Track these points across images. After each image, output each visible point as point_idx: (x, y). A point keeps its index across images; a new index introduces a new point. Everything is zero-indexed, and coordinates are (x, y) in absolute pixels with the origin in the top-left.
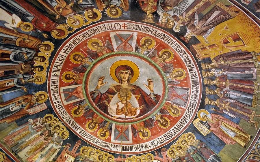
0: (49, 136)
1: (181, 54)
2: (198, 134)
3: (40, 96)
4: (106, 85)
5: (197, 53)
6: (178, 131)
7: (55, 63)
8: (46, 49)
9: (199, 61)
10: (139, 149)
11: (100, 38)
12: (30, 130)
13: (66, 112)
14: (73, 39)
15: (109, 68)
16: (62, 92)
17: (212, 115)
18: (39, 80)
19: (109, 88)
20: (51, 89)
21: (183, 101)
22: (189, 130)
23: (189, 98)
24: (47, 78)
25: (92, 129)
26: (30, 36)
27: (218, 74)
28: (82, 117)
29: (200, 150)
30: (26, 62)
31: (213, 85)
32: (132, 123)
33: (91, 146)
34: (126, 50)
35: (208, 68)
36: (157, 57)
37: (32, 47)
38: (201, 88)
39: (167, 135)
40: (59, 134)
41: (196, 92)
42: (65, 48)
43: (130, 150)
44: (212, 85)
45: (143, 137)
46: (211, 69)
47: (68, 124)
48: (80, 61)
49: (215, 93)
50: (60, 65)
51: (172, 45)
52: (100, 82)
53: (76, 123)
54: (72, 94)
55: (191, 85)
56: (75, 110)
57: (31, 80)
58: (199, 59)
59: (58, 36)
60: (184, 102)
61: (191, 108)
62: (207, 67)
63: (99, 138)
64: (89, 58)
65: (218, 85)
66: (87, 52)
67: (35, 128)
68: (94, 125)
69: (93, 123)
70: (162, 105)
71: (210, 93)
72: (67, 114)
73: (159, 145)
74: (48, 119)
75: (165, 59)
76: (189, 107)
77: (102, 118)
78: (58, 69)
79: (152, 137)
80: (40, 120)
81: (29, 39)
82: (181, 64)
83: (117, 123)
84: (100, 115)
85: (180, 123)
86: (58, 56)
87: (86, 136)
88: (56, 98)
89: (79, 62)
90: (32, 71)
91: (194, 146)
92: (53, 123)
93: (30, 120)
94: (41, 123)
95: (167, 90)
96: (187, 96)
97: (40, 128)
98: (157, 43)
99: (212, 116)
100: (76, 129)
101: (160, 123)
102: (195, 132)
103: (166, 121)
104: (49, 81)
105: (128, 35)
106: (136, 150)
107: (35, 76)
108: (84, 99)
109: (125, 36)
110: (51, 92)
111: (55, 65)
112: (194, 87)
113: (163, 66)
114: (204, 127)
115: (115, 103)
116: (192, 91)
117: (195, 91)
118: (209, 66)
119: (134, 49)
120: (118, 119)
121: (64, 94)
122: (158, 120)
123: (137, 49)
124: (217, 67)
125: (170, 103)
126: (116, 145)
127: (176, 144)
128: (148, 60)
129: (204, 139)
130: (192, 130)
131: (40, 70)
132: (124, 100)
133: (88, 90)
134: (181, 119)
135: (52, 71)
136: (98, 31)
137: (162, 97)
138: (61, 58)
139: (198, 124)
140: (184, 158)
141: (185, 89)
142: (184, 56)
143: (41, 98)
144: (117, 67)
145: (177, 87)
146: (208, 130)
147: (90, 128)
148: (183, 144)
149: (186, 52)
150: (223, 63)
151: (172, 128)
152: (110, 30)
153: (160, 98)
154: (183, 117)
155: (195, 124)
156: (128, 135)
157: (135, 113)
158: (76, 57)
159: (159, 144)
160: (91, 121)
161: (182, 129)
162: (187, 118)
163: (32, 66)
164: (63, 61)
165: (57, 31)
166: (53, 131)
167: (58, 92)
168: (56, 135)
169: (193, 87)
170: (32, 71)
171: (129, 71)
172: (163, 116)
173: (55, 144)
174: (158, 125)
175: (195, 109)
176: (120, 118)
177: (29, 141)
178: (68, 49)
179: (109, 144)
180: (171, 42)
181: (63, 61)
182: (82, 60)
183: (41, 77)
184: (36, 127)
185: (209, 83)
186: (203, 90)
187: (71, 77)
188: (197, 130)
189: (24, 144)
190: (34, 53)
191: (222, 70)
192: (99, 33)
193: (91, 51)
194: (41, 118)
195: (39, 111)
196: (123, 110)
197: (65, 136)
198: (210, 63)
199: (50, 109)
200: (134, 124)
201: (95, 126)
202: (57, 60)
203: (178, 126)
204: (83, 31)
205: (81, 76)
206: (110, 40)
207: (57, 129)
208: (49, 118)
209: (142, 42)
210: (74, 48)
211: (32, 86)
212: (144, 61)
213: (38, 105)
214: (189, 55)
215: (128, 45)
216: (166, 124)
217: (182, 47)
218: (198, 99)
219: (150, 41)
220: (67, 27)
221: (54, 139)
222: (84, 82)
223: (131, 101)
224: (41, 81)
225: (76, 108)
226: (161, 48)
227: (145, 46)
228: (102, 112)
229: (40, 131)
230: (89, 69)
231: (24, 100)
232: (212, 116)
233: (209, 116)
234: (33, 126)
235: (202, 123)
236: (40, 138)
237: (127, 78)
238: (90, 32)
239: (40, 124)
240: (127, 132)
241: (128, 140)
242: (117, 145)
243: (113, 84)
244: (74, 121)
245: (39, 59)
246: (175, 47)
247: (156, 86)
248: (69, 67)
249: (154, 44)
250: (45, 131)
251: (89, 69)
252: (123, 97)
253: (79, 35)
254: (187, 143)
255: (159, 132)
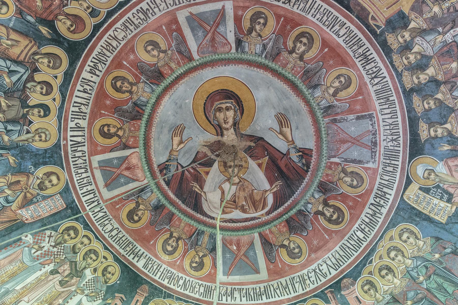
0: (71, 276)
1: (334, 29)
2: (425, 223)
3: (48, 177)
4: (190, 144)
5: (369, 13)
6: (371, 230)
7: (75, 99)
8: (51, 65)
9: (378, 31)
10: (287, 290)
11: (158, 30)
12: (26, 260)
13: (111, 217)
14: (105, 38)
15: (189, 101)
16: (96, 168)
17: (446, 163)
18: (43, 138)
19: (198, 152)
20: (71, 160)
21: (366, 150)
22: (399, 219)
23: (380, 138)
24: (60, 132)
25: (171, 253)
26: (11, 31)
27: (432, 47)
28: (146, 227)
29: (441, 263)
30: (8, 94)
31: (429, 82)
32: (261, 230)
33: (170, 296)
34: (218, 51)
35: (405, 41)
36: (285, 54)
37: (19, 59)
38: (400, 102)
39: (349, 245)
40: (95, 270)
41: (391, 118)
42: (92, 61)
43: (264, 297)
44: (425, 85)
45: (291, 258)
46: (413, 39)
47: (118, 247)
48: (127, 92)
49: (440, 103)
50: (85, 103)
51: (311, 14)
52: (176, 140)
53: (135, 243)
54: (119, 172)
55: (377, 103)
56: (129, 212)
57: (24, 137)
58: (378, 27)
59: (71, 32)
60: (370, 151)
61: (388, 161)
62: (401, 40)
63: (187, 275)
64: (145, 82)
65: (440, 78)
66: (137, 68)
67: (38, 256)
68: (174, 244)
69: (172, 240)
70: (320, 174)
71: (426, 106)
72: (111, 222)
73: (334, 273)
74: (69, 235)
75: (304, 53)
76: (384, 161)
77: (192, 224)
78: (82, 112)
79: (313, 256)
80: (50, 237)
81: (10, 37)
82: (341, 54)
83: (226, 233)
84: (185, 218)
85: (373, 208)
86: (79, 83)
87: (159, 274)
88: (85, 182)
89: (126, 96)
90: (25, 116)
91: (422, 257)
92: (82, 243)
93: (26, 236)
94: (53, 244)
95: (323, 132)
96: (373, 134)
97: (51, 256)
98: (278, 17)
99: (449, 166)
100: (136, 259)
101: (325, 218)
102: (415, 221)
103: (337, 209)
104: (64, 139)
105: (214, 11)
106: (280, 295)
107: (33, 128)
108: (146, 181)
109: (208, 15)
110: (72, 166)
111: (75, 102)
112: (384, 107)
113: (304, 74)
114: (436, 201)
115: (215, 186)
116: (381, 117)
117: (389, 116)
118: (404, 34)
119: (234, 46)
120: (226, 224)
121: (101, 171)
122: (318, 213)
123: (239, 42)
124: (425, 30)
125: (338, 164)
126: (229, 287)
127: (376, 262)
128: (267, 66)
129: (445, 232)
130: (406, 216)
131: (42, 113)
132: (235, 177)
133: (154, 160)
134: (373, 195)
135: (70, 116)
136: (151, 14)
137: (317, 152)
138: (86, 87)
139: (418, 197)
140: (405, 294)
141: (363, 117)
142: (342, 32)
143: (50, 181)
144: (205, 97)
145: (344, 120)
146: (449, 205)
147: (167, 251)
148: (393, 259)
149: (345, 21)
150: (436, 9)
151: (357, 225)
152: (177, 7)
153: (311, 156)
154: (375, 190)
155: (409, 198)
156: (256, 259)
157: (262, 204)
158: (119, 84)
159: (331, 270)
160: (168, 236)
161: (381, 221)
162: (385, 190)
163: (24, 103)
164: (91, 94)
165: (68, 19)
166: (81, 264)
167: (88, 168)
168: (88, 272)
169: (381, 107)
170: (25, 116)
171: (232, 103)
172: (329, 198)
173: (86, 295)
174: (321, 225)
175: (400, 163)
176: (231, 220)
177: (23, 287)
178: (99, 65)
179: (213, 288)
180: (308, 6)
181: (91, 94)
182: (132, 89)
183: (47, 130)
184: (41, 254)
185: (416, 81)
186: (407, 107)
187: (113, 130)
188: (419, 214)
189: (10, 296)
190: (25, 73)
191: (440, 29)
192: (155, 17)
193: (146, 63)
194: (53, 233)
195: (47, 214)
196: (235, 202)
197: (109, 276)
198: (405, 26)
199: (71, 208)
200: (266, 230)
201: (178, 247)
202: (78, 90)
203: (368, 216)
204: (121, 16)
205: (134, 127)
206: (179, 30)
207: (91, 258)
208: (72, 232)
209: (246, 24)
210: (110, 60)
211: (27, 152)
212: (258, 70)
213: (45, 198)
214: (353, 27)
215: (219, 39)
216: (338, 218)
217: (332, 10)
218: (401, 135)
219: (262, 17)
220: (88, 8)
221: (84, 283)
222: (141, 142)
223: (251, 177)
224: (46, 141)
225: (132, 205)
226: (289, 27)
227: (254, 34)
228: (189, 210)
229: (51, 263)
230: (148, 110)
231: (10, 185)
232: (449, 166)
233: (441, 168)
234: (33, 251)
235: (426, 190)
236: (51, 280)
237: (231, 121)
238: (136, 18)
239: (51, 246)
240: (251, 253)
241: (257, 271)
242: (233, 287)
243: (205, 140)
244: (129, 238)
245: (38, 88)
246: (318, 16)
247: (297, 128)
248: (106, 108)
249: (272, 22)
250: (62, 263)
251: (148, 110)
252: (230, 170)
253: (115, 26)
254: (403, 253)
255: (327, 242)
